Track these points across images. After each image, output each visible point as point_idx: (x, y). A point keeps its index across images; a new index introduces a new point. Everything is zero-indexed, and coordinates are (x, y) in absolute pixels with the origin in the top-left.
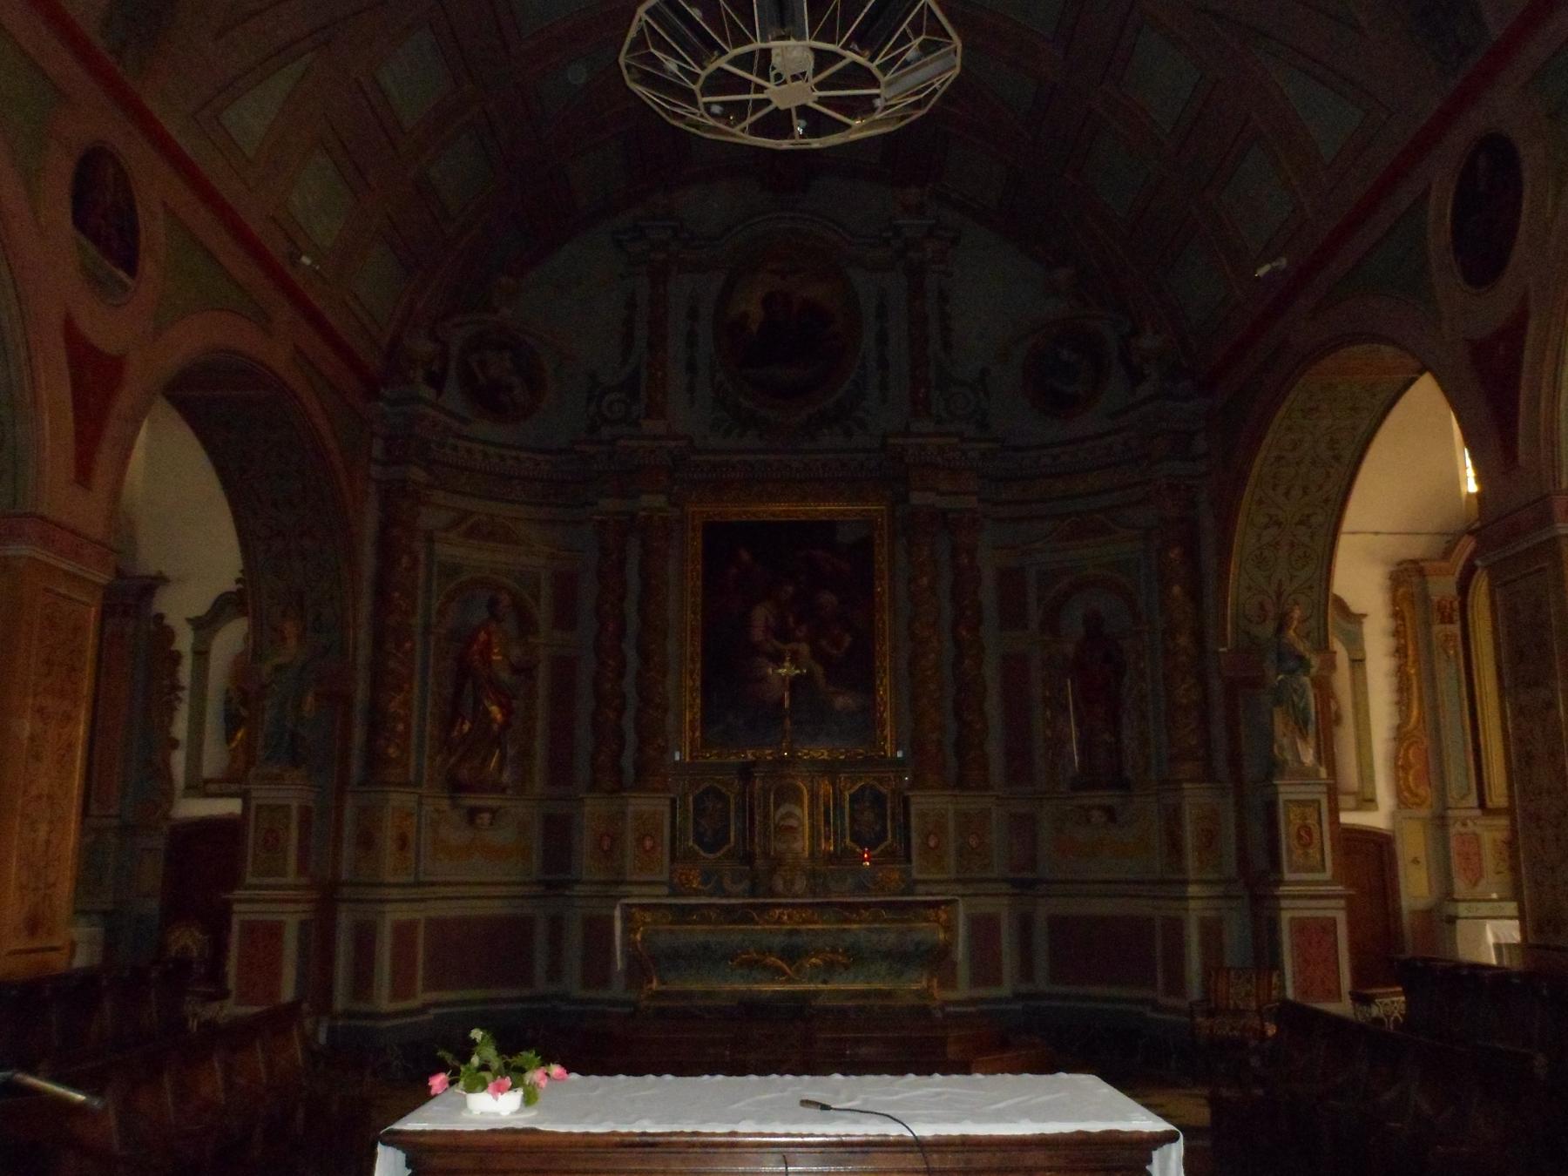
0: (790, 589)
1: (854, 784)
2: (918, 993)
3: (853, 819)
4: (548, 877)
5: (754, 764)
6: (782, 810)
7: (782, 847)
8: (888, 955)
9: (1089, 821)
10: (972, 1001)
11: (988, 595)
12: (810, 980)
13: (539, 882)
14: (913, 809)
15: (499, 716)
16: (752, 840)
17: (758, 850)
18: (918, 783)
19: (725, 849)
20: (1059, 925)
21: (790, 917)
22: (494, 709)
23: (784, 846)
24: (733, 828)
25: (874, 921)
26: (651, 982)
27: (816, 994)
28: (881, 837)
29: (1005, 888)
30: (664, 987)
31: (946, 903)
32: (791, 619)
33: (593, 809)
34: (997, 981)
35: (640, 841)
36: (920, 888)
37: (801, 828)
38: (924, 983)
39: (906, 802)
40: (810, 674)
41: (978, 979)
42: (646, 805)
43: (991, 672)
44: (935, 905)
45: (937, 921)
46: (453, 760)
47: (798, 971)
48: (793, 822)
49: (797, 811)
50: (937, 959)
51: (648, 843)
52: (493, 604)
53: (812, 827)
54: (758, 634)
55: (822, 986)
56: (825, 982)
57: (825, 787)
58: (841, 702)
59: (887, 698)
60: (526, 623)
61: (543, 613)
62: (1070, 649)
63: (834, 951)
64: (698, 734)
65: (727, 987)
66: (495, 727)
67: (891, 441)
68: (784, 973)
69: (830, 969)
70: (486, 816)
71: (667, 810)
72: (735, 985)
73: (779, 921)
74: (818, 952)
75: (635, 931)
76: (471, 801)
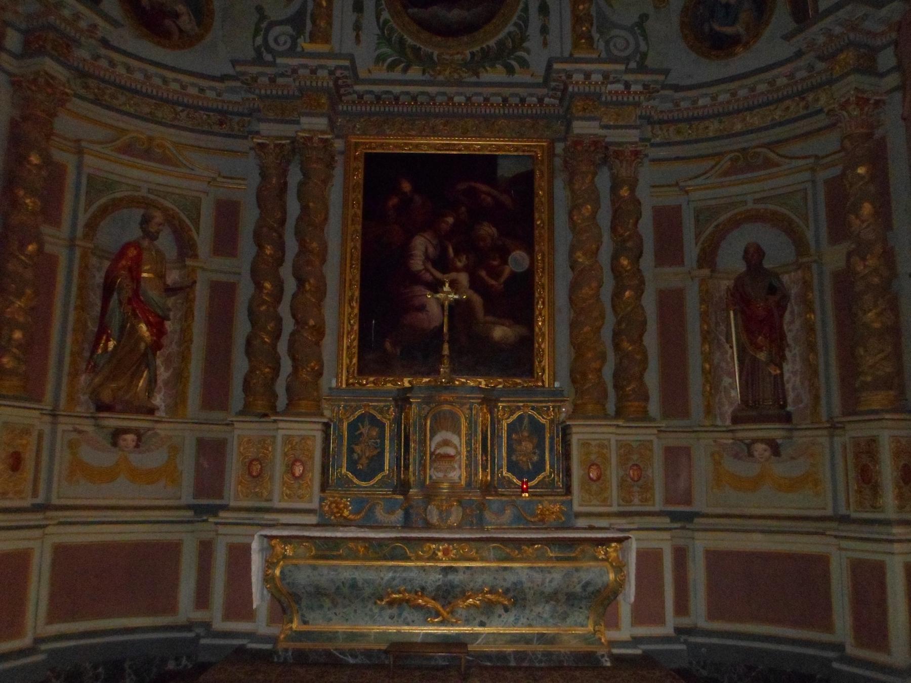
0: (450, 220)
1: (512, 413)
2: (584, 638)
3: (511, 451)
4: (196, 502)
5: (410, 389)
6: (438, 438)
8: (552, 597)
9: (751, 455)
10: (636, 641)
12: (467, 622)
13: (188, 507)
14: (574, 439)
15: (147, 334)
16: (407, 467)
17: (412, 479)
18: (577, 412)
19: (379, 477)
20: (715, 558)
23: (441, 475)
24: (387, 455)
26: (291, 621)
27: (476, 636)
28: (539, 467)
29: (665, 521)
31: (619, 540)
32: (451, 250)
33: (244, 433)
35: (290, 469)
36: (582, 522)
39: (566, 432)
42: (308, 430)
46: (97, 380)
48: (451, 451)
49: (455, 439)
50: (602, 600)
52: (146, 221)
53: (469, 457)
54: (418, 264)
56: (482, 624)
58: (499, 332)
60: (186, 248)
61: (204, 238)
62: (726, 284)
64: (355, 360)
65: (376, 629)
66: (143, 346)
67: (556, 66)
69: (488, 610)
71: (319, 436)
73: (433, 557)
76: (113, 421)
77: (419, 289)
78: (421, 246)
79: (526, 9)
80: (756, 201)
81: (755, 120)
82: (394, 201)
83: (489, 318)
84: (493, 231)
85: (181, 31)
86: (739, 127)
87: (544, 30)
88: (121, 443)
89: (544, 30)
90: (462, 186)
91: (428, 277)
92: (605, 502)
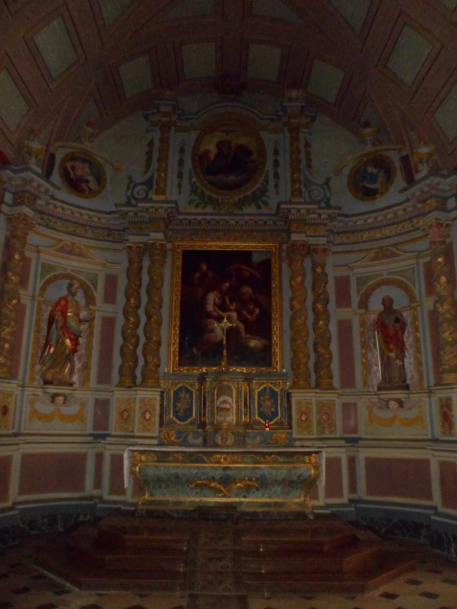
0: (227, 285)
1: (260, 386)
3: (260, 406)
4: (95, 432)
5: (206, 374)
6: (221, 399)
7: (221, 419)
10: (327, 506)
11: (331, 288)
12: (237, 496)
13: (90, 435)
14: (294, 400)
16: (205, 415)
17: (207, 421)
18: (295, 385)
19: (190, 419)
20: (371, 463)
21: (225, 459)
22: (68, 341)
23: (222, 419)
24: (194, 408)
25: (274, 462)
26: (145, 495)
27: (242, 503)
28: (275, 414)
29: (343, 443)
30: (152, 499)
32: (227, 300)
33: (118, 397)
34: (341, 495)
36: (298, 443)
37: (230, 409)
38: (302, 499)
39: (289, 395)
40: (237, 326)
41: (329, 493)
43: (333, 328)
44: (309, 454)
45: (310, 463)
47: (229, 491)
48: (228, 406)
49: (230, 400)
50: (308, 485)
51: (148, 416)
54: (210, 307)
55: (243, 500)
56: (245, 497)
57: (244, 387)
59: (278, 341)
60: (90, 300)
61: (99, 295)
63: (250, 480)
64: (177, 358)
65: (189, 499)
67: (282, 206)
68: (221, 492)
69: (248, 489)
70: (61, 398)
71: (158, 398)
72: (192, 499)
73: (218, 462)
74: (241, 480)
75: (136, 465)
76: (52, 390)
77: (211, 321)
78: (212, 298)
79: (267, 176)
80: (388, 274)
81: (387, 232)
82: (198, 275)
83: (248, 336)
84: (250, 290)
85: (90, 189)
86: (378, 236)
87: (277, 186)
88: (56, 401)
89: (277, 186)
90: (233, 267)
91: (215, 314)
92: (310, 433)
